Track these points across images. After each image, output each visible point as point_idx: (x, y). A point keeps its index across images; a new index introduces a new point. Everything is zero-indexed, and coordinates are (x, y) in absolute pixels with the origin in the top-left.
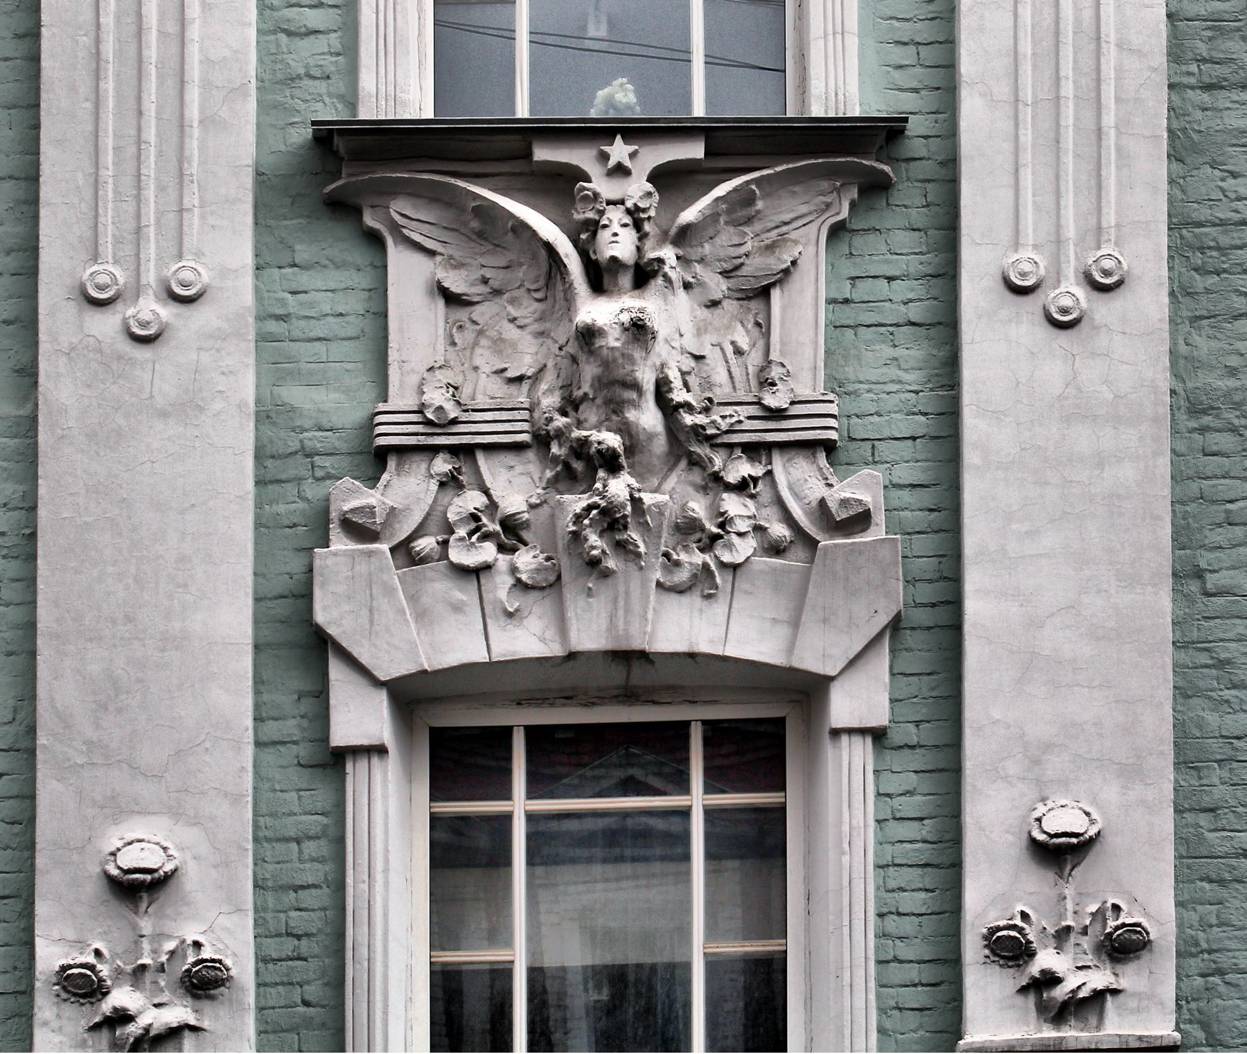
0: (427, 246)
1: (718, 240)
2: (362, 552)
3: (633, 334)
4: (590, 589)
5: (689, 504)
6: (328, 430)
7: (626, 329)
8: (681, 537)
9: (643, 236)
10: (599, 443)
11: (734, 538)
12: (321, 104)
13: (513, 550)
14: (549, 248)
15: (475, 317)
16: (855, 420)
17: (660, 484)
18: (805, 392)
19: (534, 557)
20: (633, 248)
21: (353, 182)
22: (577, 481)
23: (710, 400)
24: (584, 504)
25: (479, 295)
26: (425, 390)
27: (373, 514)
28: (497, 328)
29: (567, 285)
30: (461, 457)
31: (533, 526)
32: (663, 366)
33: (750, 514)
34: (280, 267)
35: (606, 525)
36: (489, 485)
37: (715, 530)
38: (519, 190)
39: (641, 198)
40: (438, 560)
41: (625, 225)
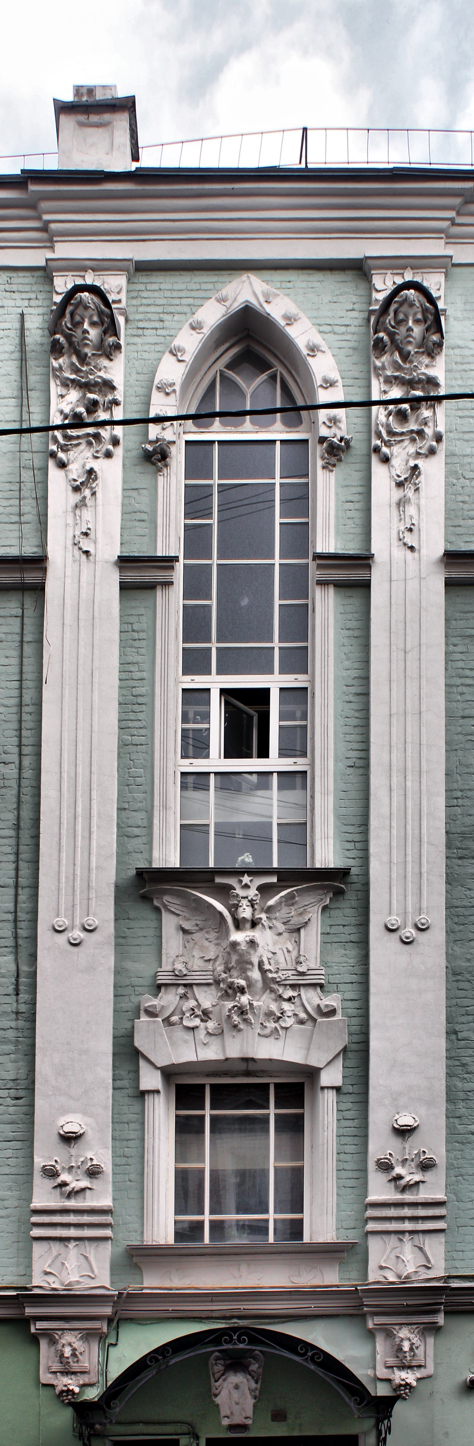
1: (281, 911)
9: (254, 910)
13: (206, 1021)
16: (331, 976)
18: (313, 966)
23: (278, 968)
24: (232, 1005)
27: (156, 1008)
32: (261, 956)
37: (280, 1015)
41: (248, 906)
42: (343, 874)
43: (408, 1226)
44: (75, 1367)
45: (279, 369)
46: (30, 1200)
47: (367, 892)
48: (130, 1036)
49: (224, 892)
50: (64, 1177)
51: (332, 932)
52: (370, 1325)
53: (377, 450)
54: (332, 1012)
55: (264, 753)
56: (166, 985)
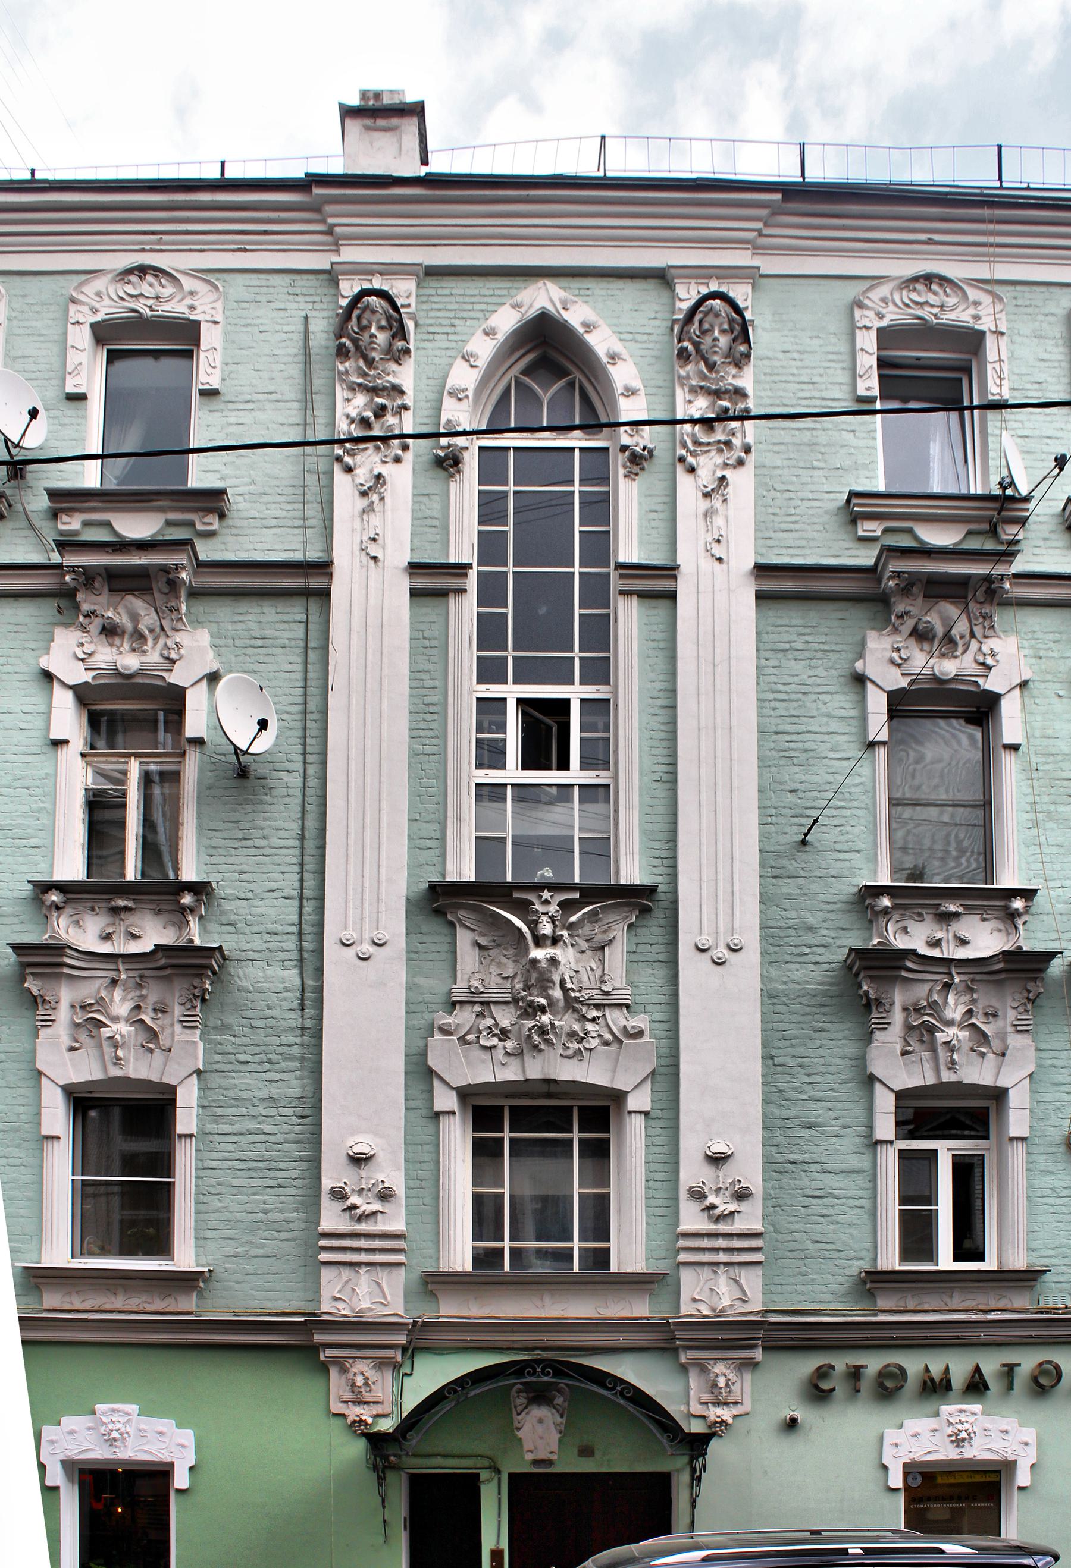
9: (555, 926)
14: (519, 930)
18: (618, 986)
42: (649, 891)
43: (722, 1257)
44: (368, 1397)
45: (577, 375)
46: (318, 1224)
47: (676, 910)
48: (424, 1054)
49: (523, 908)
50: (354, 1199)
52: (683, 1359)
53: (682, 460)
54: (640, 1034)
55: (564, 765)
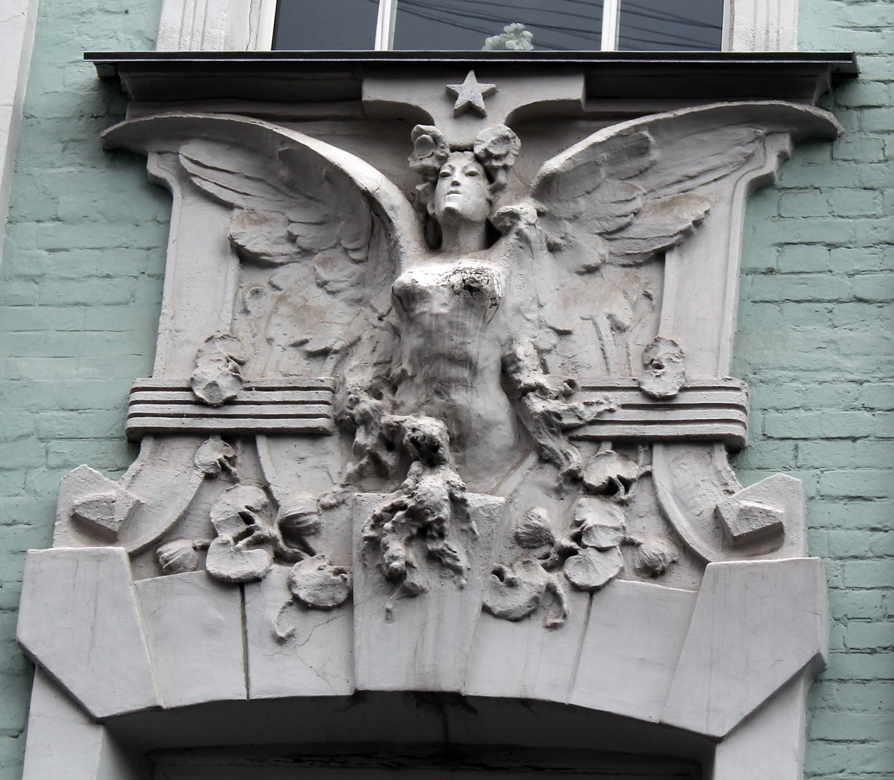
0: (222, 198)
1: (597, 196)
2: (89, 555)
3: (465, 298)
4: (388, 611)
5: (535, 511)
6: (72, 410)
7: (457, 293)
8: (522, 551)
9: (497, 189)
10: (414, 430)
11: (592, 554)
12: (114, 40)
13: (293, 560)
14: (370, 199)
15: (276, 281)
16: (773, 414)
17: (498, 486)
18: (698, 377)
19: (319, 569)
20: (482, 201)
21: (135, 124)
22: (389, 479)
23: (571, 383)
24: (387, 504)
25: (283, 255)
26: (199, 364)
27: (111, 510)
28: (303, 294)
29: (393, 243)
30: (239, 445)
31: (324, 532)
32: (511, 340)
33: (616, 525)
34: (38, 221)
35: (414, 531)
36: (269, 480)
37: (567, 542)
38: (348, 137)
39: (494, 142)
40: (195, 570)
41: (472, 174)
51: (784, 266)
56: (160, 435)
